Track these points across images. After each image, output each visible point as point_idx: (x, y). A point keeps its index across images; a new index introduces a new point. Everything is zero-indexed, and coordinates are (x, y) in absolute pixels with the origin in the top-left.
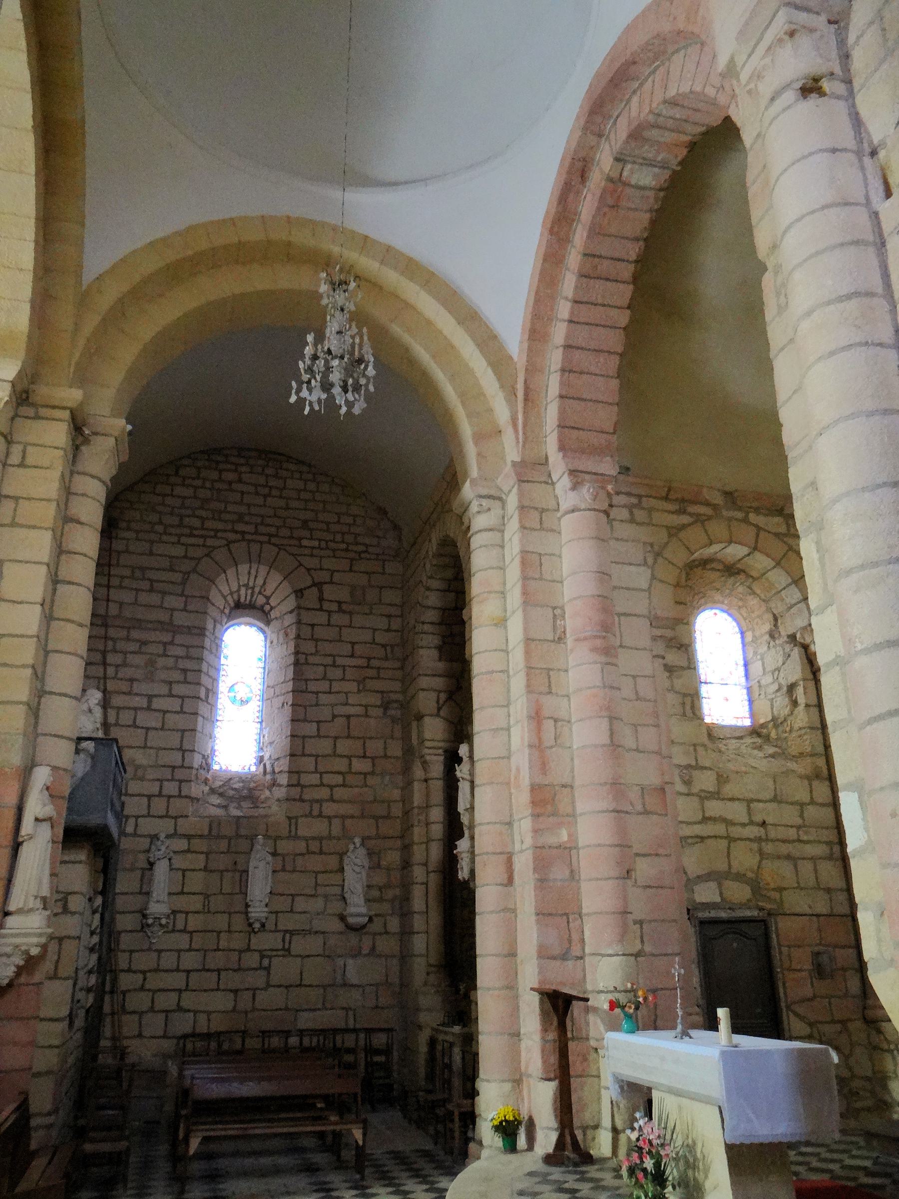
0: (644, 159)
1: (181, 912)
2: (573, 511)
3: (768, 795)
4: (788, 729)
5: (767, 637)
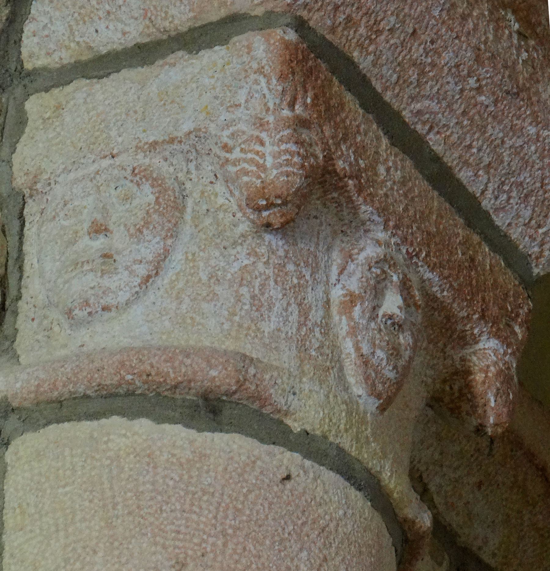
2: (210, 409)
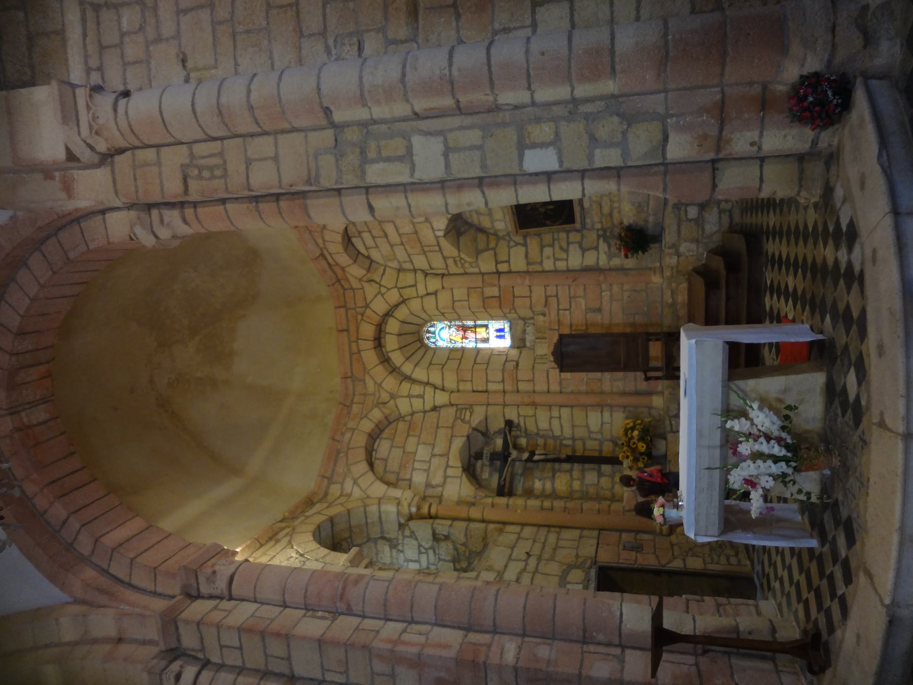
0: (29, 403)
1: (555, 393)
3: (509, 551)
4: (463, 548)
5: (394, 552)
